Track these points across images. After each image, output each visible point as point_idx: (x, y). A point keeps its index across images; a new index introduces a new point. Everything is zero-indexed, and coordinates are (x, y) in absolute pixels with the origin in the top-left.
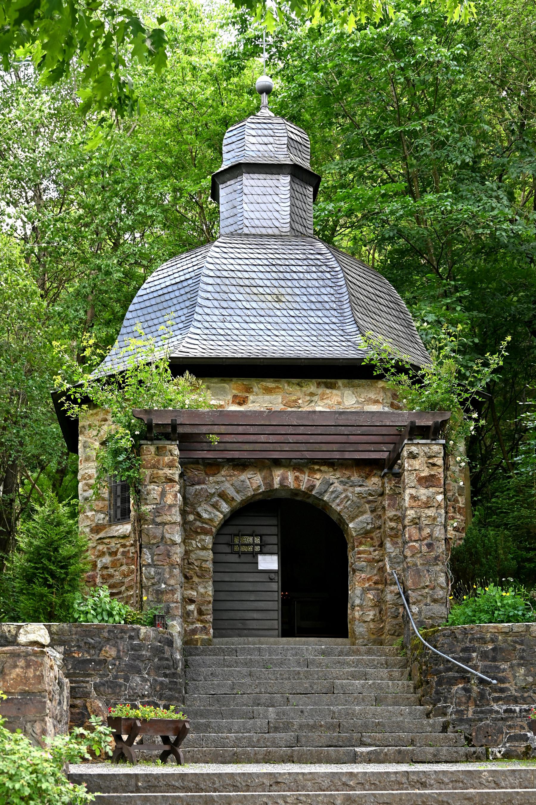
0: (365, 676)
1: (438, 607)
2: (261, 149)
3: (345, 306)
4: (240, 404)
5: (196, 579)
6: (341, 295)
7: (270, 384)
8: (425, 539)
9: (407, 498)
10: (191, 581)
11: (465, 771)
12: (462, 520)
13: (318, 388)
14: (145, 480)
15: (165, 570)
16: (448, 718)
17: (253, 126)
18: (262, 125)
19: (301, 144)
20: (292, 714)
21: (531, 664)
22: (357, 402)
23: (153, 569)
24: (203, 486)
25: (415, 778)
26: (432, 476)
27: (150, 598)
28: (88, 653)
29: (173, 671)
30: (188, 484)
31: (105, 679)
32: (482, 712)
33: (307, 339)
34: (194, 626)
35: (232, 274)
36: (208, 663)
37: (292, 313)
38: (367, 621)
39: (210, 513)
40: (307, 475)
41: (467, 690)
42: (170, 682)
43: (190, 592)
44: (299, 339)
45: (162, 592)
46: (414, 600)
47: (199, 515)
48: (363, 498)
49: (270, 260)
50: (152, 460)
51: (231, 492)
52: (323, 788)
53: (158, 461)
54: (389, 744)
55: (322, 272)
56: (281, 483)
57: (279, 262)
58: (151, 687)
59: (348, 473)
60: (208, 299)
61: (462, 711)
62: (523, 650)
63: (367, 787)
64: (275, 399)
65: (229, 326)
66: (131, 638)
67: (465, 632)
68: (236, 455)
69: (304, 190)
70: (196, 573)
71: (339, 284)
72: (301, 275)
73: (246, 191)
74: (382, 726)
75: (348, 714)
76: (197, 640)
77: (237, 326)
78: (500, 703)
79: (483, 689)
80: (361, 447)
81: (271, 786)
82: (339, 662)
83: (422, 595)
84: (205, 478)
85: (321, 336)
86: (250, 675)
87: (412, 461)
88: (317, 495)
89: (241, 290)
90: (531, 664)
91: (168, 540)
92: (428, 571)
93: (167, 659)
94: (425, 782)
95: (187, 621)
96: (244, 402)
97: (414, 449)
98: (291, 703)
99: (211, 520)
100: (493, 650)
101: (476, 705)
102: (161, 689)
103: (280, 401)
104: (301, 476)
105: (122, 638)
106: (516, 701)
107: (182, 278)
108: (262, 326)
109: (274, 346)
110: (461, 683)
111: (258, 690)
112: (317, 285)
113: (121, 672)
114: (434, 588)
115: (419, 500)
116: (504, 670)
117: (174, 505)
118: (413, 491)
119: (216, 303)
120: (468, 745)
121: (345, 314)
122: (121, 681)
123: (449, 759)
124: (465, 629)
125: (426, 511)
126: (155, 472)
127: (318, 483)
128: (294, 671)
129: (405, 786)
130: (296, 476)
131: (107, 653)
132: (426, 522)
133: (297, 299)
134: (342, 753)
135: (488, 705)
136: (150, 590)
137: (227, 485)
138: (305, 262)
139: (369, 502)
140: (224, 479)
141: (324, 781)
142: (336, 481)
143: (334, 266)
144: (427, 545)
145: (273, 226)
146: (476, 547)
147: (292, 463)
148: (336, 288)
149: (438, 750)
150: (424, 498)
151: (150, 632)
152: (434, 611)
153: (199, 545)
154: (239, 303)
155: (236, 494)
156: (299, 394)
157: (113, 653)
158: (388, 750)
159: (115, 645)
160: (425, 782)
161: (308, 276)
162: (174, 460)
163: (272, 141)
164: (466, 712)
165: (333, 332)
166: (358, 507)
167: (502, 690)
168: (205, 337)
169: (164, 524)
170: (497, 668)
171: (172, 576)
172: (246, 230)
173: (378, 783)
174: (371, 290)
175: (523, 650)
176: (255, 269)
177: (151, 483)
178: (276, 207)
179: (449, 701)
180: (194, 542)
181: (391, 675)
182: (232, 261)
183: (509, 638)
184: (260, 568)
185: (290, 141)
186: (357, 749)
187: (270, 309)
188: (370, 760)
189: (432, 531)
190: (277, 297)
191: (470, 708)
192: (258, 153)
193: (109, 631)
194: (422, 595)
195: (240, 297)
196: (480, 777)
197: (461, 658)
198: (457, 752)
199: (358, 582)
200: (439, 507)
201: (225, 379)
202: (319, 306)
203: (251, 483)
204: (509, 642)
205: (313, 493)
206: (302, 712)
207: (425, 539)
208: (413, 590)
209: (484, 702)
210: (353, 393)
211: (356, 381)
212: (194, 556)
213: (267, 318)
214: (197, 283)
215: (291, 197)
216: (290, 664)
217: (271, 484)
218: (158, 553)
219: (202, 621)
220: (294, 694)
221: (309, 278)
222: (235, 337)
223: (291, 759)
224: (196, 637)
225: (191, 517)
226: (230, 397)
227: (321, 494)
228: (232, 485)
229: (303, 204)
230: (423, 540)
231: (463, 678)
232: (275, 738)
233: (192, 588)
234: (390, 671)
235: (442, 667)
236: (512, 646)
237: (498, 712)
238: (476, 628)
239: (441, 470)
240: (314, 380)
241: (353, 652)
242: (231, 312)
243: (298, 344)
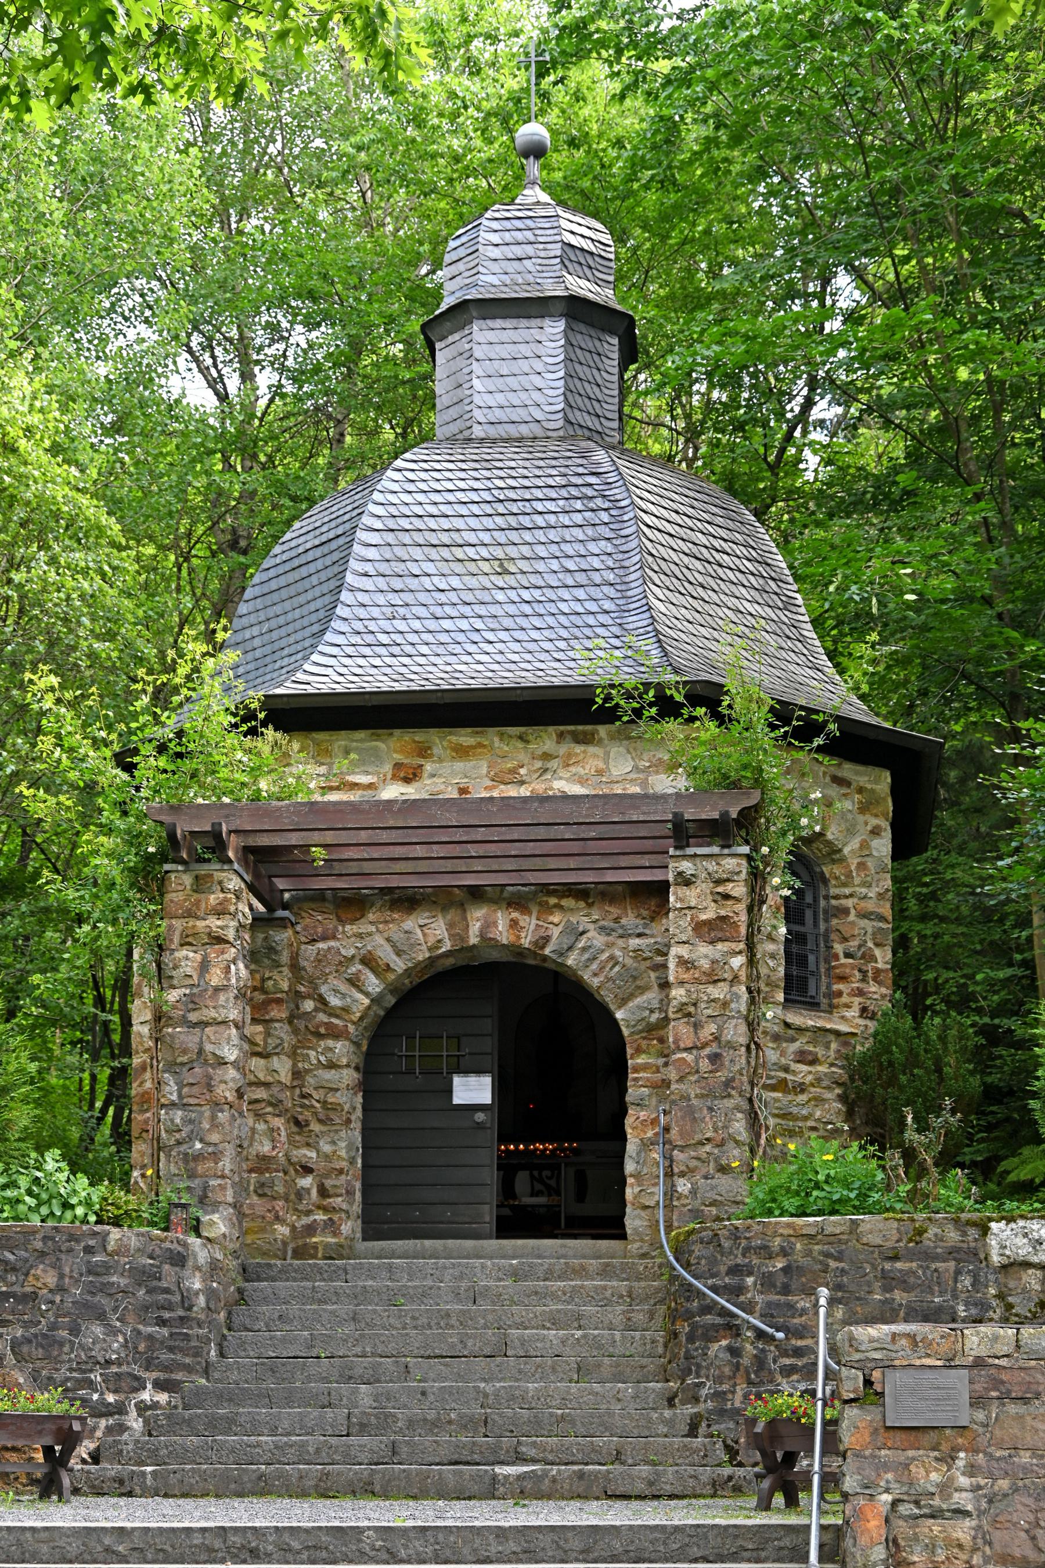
0: (578, 1321)
1: (730, 1181)
2: (510, 270)
3: (632, 577)
4: (407, 780)
6: (627, 555)
7: (465, 737)
10: (306, 1129)
11: (332, 1528)
12: (883, 996)
13: (558, 742)
14: (171, 940)
15: (202, 1113)
16: (700, 1408)
17: (495, 225)
18: (514, 222)
19: (592, 254)
20: (404, 1399)
21: (858, 1299)
22: (636, 769)
23: (180, 1113)
24: (332, 943)
25: (237, 1540)
26: (723, 919)
27: (174, 1169)
29: (181, 1313)
30: (303, 939)
31: (32, 1331)
33: (547, 646)
34: (312, 1218)
35: (418, 523)
36: (283, 1294)
37: (526, 595)
38: (648, 1207)
39: (344, 996)
40: (534, 916)
41: (734, 1352)
42: (171, 1335)
43: (305, 1151)
44: (531, 646)
45: (198, 1157)
46: (683, 1168)
47: (322, 1000)
48: (645, 959)
49: (495, 492)
50: (185, 900)
51: (386, 954)
53: (197, 903)
54: (571, 1459)
55: (593, 510)
56: (482, 935)
57: (512, 494)
58: (125, 1345)
59: (615, 911)
60: (366, 575)
61: (724, 1393)
62: (843, 1270)
63: (150, 1556)
64: (474, 767)
65: (401, 625)
66: (89, 1250)
68: (394, 882)
69: (597, 343)
70: (315, 1114)
71: (623, 533)
72: (552, 519)
73: (478, 353)
74: (570, 1422)
75: (513, 1398)
76: (315, 1247)
77: (417, 625)
78: (795, 1377)
79: (763, 1351)
80: (624, 861)
82: (536, 1293)
83: (698, 1159)
84: (336, 928)
85: (576, 638)
86: (354, 1319)
87: (683, 891)
88: (554, 956)
89: (433, 553)
90: (858, 1299)
91: (210, 1056)
92: (711, 1109)
93: (167, 1291)
94: (257, 1548)
95: (296, 1210)
96: (415, 775)
97: (686, 867)
98: (412, 1375)
99: (346, 1010)
100: (786, 1270)
101: (750, 1383)
102: (149, 1348)
103: (484, 771)
104: (524, 920)
105: (70, 1251)
107: (331, 535)
108: (464, 624)
109: (480, 663)
110: (725, 1337)
111: (358, 1350)
112: (581, 537)
113: (65, 1316)
114: (721, 1145)
115: (695, 968)
117: (224, 988)
118: (683, 951)
119: (381, 583)
120: (730, 1462)
121: (630, 593)
122: (64, 1333)
123: (678, 1490)
124: (737, 1228)
125: (710, 989)
126: (190, 924)
127: (555, 932)
128: (439, 1311)
129: (220, 1555)
130: (512, 920)
131: (38, 1279)
132: (709, 1012)
133: (540, 566)
134: (467, 1477)
135: (771, 1382)
136: (173, 1153)
137: (379, 940)
138: (564, 493)
140: (374, 929)
141: (70, 1544)
142: (591, 926)
143: (618, 497)
144: (709, 1057)
145: (530, 419)
146: (891, 1052)
147: (505, 895)
148: (618, 542)
149: (657, 1473)
150: (705, 964)
151: (129, 1238)
152: (722, 1190)
153: (322, 1059)
154: (426, 580)
155: (395, 957)
156: (523, 757)
157: (51, 1280)
158: (559, 1471)
160: (257, 1548)
161: (565, 519)
162: (226, 900)
163: (531, 253)
164: (730, 1396)
165: (600, 631)
166: (635, 978)
167: (798, 1352)
168: (350, 650)
169: (203, 1024)
170: (791, 1306)
171: (215, 1125)
172: (478, 432)
173: (170, 1549)
174: (703, 539)
176: (463, 510)
177: (182, 945)
178: (538, 381)
179: (703, 1372)
180: (312, 1053)
181: (629, 1319)
182: (420, 497)
183: (816, 1247)
184: (457, 1100)
185: (566, 248)
186: (498, 1469)
187: (485, 589)
188: (522, 1492)
189: (720, 1029)
190: (501, 565)
191: (738, 1388)
192: (504, 277)
193: (45, 1239)
194: (698, 1159)
195: (429, 567)
196: (360, 1541)
197: (725, 1287)
198: (695, 1477)
199: (633, 1128)
200: (735, 979)
201: (380, 731)
202: (581, 578)
203: (424, 935)
204: (815, 1254)
205: (547, 951)
206: (423, 1393)
207: (705, 1045)
208: (682, 1149)
210: (629, 752)
212: (311, 1081)
213: (476, 608)
214: (350, 544)
215: (568, 359)
216: (439, 1297)
217: (463, 938)
218: (191, 1081)
219: (325, 1209)
220: (429, 1357)
221: (567, 523)
222: (409, 649)
223: (369, 1488)
224: (314, 1240)
225: (309, 1005)
226: (388, 768)
227: (561, 955)
228: (388, 940)
229: (595, 372)
230: (702, 1048)
231: (729, 1327)
232: (349, 1446)
233: (308, 1145)
234: (628, 1311)
235: (695, 1304)
236: (821, 1262)
238: (756, 1227)
239: (741, 907)
240: (551, 729)
241: (574, 1271)
242: (408, 598)
243: (528, 657)
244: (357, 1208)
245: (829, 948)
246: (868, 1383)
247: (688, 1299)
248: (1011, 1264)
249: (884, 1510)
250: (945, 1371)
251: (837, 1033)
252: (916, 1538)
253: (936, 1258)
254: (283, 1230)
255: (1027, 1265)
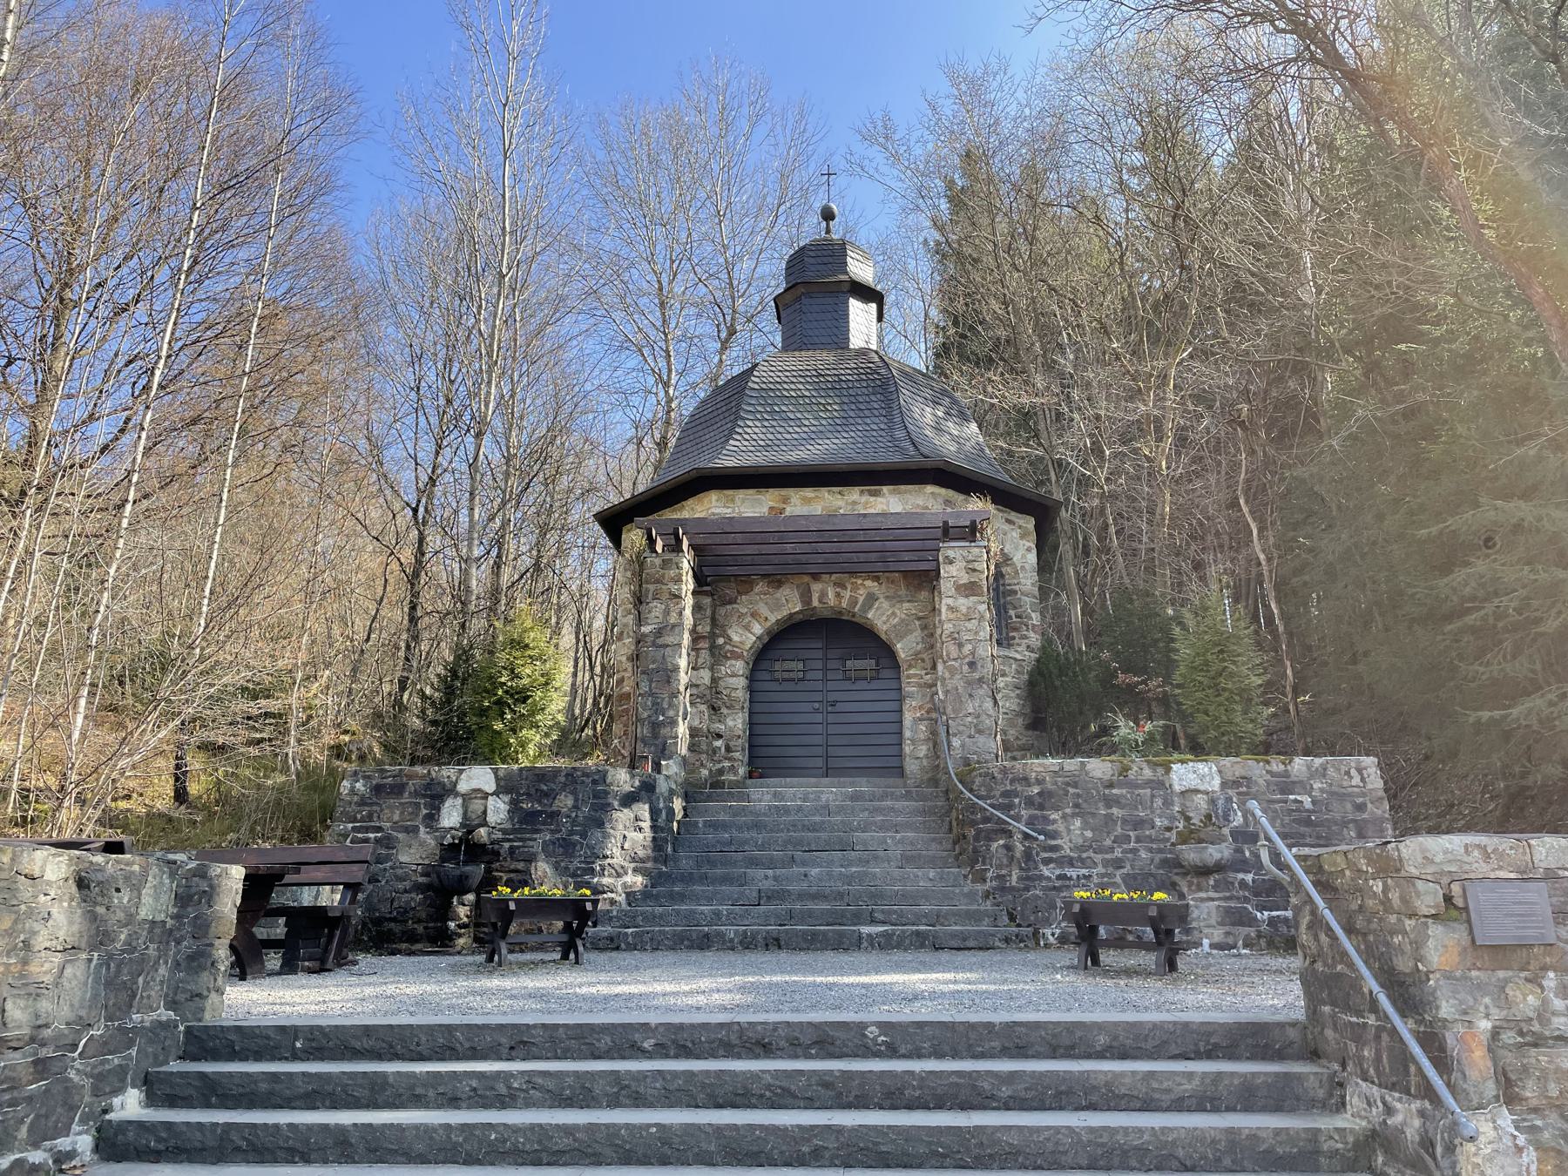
5: (724, 711)
8: (965, 657)
9: (944, 610)
28: (540, 802)
32: (1028, 878)
41: (1008, 848)
52: (596, 1053)
53: (663, 576)
67: (1004, 771)
78: (1052, 866)
81: (512, 1048)
97: (951, 553)
101: (1021, 869)
106: (1071, 863)
116: (1055, 821)
118: (950, 601)
122: (577, 838)
139: (919, 619)
141: (599, 1040)
152: (980, 745)
159: (574, 793)
170: (1046, 819)
175: (1078, 795)
189: (974, 648)
207: (965, 657)
209: (1031, 864)
211: (903, 487)
219: (730, 759)
237: (1049, 879)
244: (746, 759)
245: (1006, 612)
246: (1448, 899)
247: (972, 813)
248: (1187, 791)
249: (1484, 1038)
250: (1518, 883)
251: (1015, 659)
252: (1525, 1069)
253: (1137, 786)
254: (705, 772)
255: (1197, 791)
